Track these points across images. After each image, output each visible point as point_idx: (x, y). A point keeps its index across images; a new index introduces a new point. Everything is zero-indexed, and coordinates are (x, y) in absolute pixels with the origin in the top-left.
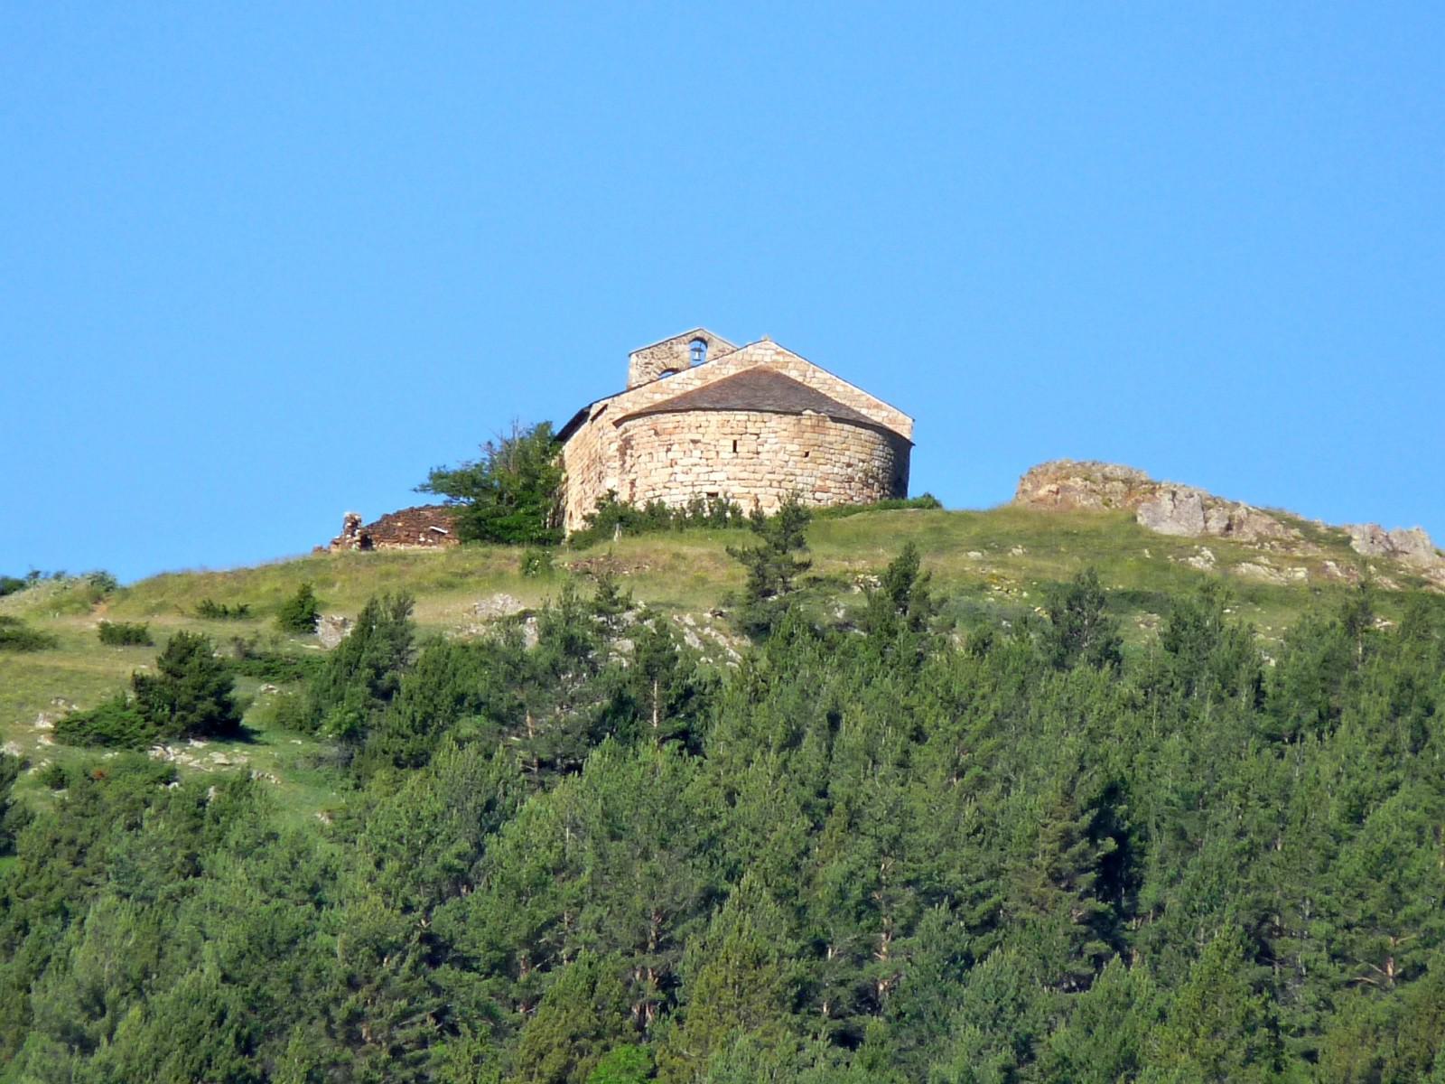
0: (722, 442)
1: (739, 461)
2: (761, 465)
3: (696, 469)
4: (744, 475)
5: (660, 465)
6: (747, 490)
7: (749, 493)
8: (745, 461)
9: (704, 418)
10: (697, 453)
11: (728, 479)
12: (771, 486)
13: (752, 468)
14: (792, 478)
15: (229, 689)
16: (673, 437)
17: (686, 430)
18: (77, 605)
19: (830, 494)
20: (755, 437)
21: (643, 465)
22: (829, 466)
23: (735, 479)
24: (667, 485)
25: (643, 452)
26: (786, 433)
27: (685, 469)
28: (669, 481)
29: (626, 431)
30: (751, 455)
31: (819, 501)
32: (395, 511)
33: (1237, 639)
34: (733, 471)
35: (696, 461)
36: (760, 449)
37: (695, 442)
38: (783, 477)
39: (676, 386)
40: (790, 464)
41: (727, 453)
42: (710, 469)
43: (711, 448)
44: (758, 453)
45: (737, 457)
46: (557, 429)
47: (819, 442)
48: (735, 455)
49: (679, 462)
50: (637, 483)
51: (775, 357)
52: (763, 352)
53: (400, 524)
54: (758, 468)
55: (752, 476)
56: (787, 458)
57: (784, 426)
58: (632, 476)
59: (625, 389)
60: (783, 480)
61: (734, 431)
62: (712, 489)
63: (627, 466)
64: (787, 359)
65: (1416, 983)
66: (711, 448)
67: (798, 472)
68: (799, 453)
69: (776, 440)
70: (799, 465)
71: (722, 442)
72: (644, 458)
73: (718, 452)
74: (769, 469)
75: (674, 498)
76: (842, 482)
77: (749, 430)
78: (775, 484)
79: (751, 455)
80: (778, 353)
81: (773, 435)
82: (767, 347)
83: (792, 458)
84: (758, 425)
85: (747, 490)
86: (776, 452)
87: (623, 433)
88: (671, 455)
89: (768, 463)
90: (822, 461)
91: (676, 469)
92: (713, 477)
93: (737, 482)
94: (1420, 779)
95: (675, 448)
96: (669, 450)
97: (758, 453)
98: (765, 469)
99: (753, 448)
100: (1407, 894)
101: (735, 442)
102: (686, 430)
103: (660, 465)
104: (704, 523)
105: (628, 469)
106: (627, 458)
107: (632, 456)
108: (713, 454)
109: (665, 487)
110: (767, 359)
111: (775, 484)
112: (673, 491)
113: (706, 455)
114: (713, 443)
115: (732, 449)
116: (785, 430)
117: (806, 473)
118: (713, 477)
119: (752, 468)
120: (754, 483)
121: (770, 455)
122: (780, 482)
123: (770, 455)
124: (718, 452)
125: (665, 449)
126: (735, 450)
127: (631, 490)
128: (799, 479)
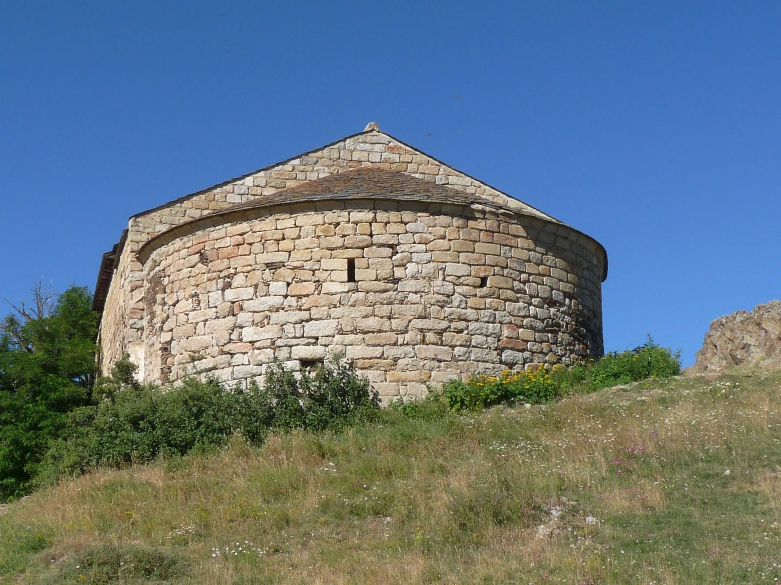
0: (325, 264)
1: (361, 295)
2: (401, 302)
3: (281, 316)
4: (372, 323)
5: (212, 313)
6: (378, 351)
8: (371, 297)
9: (290, 223)
10: (278, 287)
11: (341, 332)
12: (423, 341)
13: (386, 310)
14: (461, 325)
16: (233, 263)
17: (257, 247)
18: (232, 364)
19: (527, 354)
20: (389, 251)
21: (182, 317)
22: (521, 304)
23: (354, 332)
24: (226, 349)
25: (767, 390)
26: (444, 244)
27: (258, 317)
29: (156, 264)
30: (382, 285)
31: (511, 365)
34: (349, 315)
35: (277, 301)
36: (399, 272)
37: (270, 266)
38: (444, 324)
40: (456, 299)
41: (337, 285)
42: (305, 315)
43: (305, 275)
44: (396, 281)
46: (92, 290)
47: (501, 260)
49: (246, 305)
50: (174, 348)
52: (368, 147)
54: (396, 307)
55: (386, 325)
56: (449, 288)
57: (440, 231)
58: (165, 337)
60: (445, 330)
61: (348, 241)
62: (315, 351)
63: (157, 321)
64: (407, 158)
66: (307, 275)
67: (470, 313)
68: (471, 280)
69: (428, 256)
70: (471, 302)
71: (325, 264)
72: (186, 305)
73: (318, 283)
75: (240, 371)
76: (543, 331)
77: (375, 239)
78: (431, 337)
79: (382, 285)
80: (391, 150)
82: (374, 139)
83: (459, 289)
84: (393, 228)
85: (378, 351)
86: (430, 278)
87: (152, 269)
88: (230, 294)
89: (412, 297)
90: (510, 294)
91: (243, 317)
92: (311, 329)
93: (360, 336)
94: (449, 324)
95: (238, 280)
96: (228, 286)
97: (396, 281)
98: (409, 310)
99: (385, 272)
100: (689, 460)
102: (257, 247)
103: (212, 313)
104: (405, 344)
105: (157, 326)
106: (157, 308)
107: (164, 304)
108: (310, 287)
109: (223, 353)
110: (376, 158)
111: (431, 337)
112: (238, 359)
113: (295, 289)
114: (308, 265)
115: (345, 276)
116: (443, 237)
117: (485, 314)
118: (311, 329)
119: (386, 310)
120: (392, 336)
122: (440, 333)
124: (318, 283)
125: (221, 285)
126: (351, 278)
127: (164, 360)
128: (473, 326)
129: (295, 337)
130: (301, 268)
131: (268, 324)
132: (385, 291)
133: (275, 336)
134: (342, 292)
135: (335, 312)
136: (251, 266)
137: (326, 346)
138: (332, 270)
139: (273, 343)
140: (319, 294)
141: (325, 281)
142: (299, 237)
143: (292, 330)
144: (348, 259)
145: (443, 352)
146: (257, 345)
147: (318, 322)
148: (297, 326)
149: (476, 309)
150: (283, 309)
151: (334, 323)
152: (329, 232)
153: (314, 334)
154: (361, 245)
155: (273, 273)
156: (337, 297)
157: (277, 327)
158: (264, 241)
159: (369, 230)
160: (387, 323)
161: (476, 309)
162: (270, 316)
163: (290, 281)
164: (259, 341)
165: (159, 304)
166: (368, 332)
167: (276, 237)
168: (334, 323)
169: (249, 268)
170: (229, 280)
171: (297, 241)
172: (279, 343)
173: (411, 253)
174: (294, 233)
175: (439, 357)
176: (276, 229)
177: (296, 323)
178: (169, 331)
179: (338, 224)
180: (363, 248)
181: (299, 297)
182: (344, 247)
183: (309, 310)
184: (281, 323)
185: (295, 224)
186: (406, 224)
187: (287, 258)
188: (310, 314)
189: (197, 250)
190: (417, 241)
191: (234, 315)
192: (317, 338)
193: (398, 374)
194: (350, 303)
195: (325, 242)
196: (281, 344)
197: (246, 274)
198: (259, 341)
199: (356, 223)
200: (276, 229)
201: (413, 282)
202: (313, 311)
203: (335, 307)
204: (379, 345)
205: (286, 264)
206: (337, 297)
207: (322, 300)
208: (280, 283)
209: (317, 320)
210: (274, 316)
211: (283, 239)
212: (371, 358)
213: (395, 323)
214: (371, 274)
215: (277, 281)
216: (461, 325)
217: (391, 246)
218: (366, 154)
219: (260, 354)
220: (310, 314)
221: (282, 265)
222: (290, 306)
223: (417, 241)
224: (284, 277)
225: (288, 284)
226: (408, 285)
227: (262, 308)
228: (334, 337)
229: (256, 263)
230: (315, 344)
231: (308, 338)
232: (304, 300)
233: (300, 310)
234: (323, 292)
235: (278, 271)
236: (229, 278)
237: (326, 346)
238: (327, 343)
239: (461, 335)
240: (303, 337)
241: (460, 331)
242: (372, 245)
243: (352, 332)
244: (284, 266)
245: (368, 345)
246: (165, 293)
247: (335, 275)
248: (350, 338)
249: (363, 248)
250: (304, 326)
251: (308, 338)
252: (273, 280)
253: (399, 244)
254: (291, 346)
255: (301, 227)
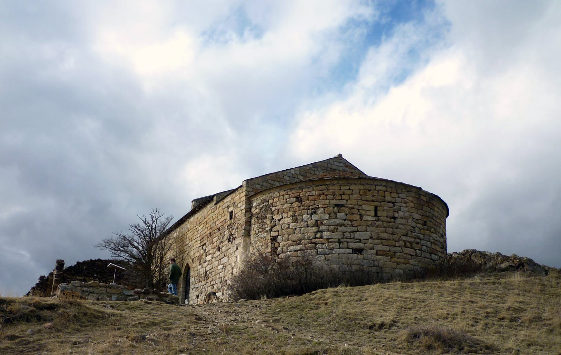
1: (381, 223)
4: (385, 235)
6: (387, 248)
7: (390, 251)
8: (385, 224)
11: (371, 238)
12: (405, 246)
15: (63, 264)
20: (391, 205)
23: (378, 238)
27: (331, 228)
28: (316, 238)
32: (83, 261)
33: (454, 291)
36: (396, 215)
37: (337, 206)
39: (288, 178)
41: (370, 218)
42: (355, 229)
44: (394, 218)
45: (378, 221)
48: (376, 218)
51: (345, 168)
53: (85, 267)
55: (391, 237)
59: (189, 208)
65: (301, 297)
66: (356, 211)
67: (421, 236)
71: (364, 207)
73: (361, 216)
74: (404, 232)
81: (404, 205)
85: (387, 248)
88: (315, 217)
89: (402, 226)
92: (357, 235)
93: (380, 241)
95: (320, 211)
96: (315, 213)
99: (390, 214)
101: (376, 208)
108: (358, 217)
113: (350, 217)
114: (356, 207)
115: (373, 214)
118: (357, 235)
121: (403, 221)
122: (411, 243)
123: (403, 221)
124: (361, 216)
126: (376, 215)
128: (423, 242)
129: (350, 239)
130: (353, 208)
131: (337, 231)
132: (390, 222)
133: (340, 237)
134: (372, 221)
135: (369, 229)
136: (327, 205)
137: (365, 243)
138: (368, 210)
139: (339, 240)
140: (361, 220)
141: (364, 215)
142: (352, 194)
143: (349, 235)
144: (375, 206)
145: (412, 251)
146: (330, 240)
147: (361, 233)
148: (352, 233)
149: (424, 235)
150: (344, 225)
151: (369, 234)
152: (366, 193)
153: (360, 238)
154: (380, 201)
155: (339, 209)
156: (370, 223)
157: (341, 233)
158: (334, 194)
159: (384, 195)
160: (391, 236)
161: (424, 235)
162: (337, 228)
163: (347, 213)
164: (331, 239)
165: (268, 219)
166: (383, 239)
167: (340, 193)
168: (369, 234)
169: (326, 206)
170: (315, 210)
171: (351, 196)
172: (342, 240)
173: (400, 207)
174: (350, 192)
175: (411, 254)
176: (340, 189)
177: (350, 232)
178: (276, 231)
179: (370, 190)
180: (381, 202)
181: (352, 221)
182: (373, 201)
183: (356, 227)
184: (344, 231)
185: (350, 188)
186: (398, 194)
187: (346, 203)
188: (357, 229)
189: (295, 196)
190: (403, 201)
191: (317, 226)
192: (360, 240)
193: (396, 259)
194: (375, 226)
195: (364, 198)
196: (343, 241)
197: (324, 208)
198: (331, 239)
199: (378, 191)
200: (340, 189)
201: (401, 220)
202: (359, 227)
203: (369, 227)
204: (388, 246)
205: (345, 205)
206: (370, 223)
207: (363, 223)
208: (343, 214)
209: (360, 232)
210: (340, 228)
211: (344, 194)
212: (385, 251)
213: (395, 237)
214: (385, 214)
215: (340, 212)
216: (418, 241)
217: (393, 203)
218: (337, 167)
219: (332, 244)
220: (357, 229)
221: (343, 206)
222: (347, 224)
223: (403, 201)
224: (345, 212)
225: (346, 215)
226: (399, 221)
227: (333, 224)
228: (368, 240)
229: (330, 204)
230: (359, 242)
231: (356, 239)
232: (354, 222)
233: (353, 226)
234: (363, 219)
235: (342, 208)
236: (314, 209)
237: (365, 243)
238: (366, 242)
239: (418, 245)
240: (354, 239)
241: (418, 243)
242: (385, 201)
243: (376, 239)
244: (344, 206)
245: (383, 245)
246: (273, 214)
247: (369, 213)
248: (376, 241)
249: (381, 202)
250: (354, 234)
251: (356, 239)
252: (339, 212)
253: (396, 202)
254: (348, 242)
255: (352, 190)
